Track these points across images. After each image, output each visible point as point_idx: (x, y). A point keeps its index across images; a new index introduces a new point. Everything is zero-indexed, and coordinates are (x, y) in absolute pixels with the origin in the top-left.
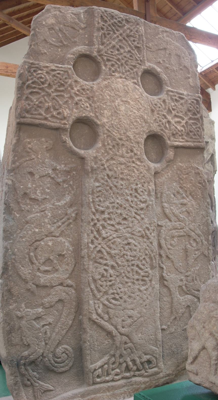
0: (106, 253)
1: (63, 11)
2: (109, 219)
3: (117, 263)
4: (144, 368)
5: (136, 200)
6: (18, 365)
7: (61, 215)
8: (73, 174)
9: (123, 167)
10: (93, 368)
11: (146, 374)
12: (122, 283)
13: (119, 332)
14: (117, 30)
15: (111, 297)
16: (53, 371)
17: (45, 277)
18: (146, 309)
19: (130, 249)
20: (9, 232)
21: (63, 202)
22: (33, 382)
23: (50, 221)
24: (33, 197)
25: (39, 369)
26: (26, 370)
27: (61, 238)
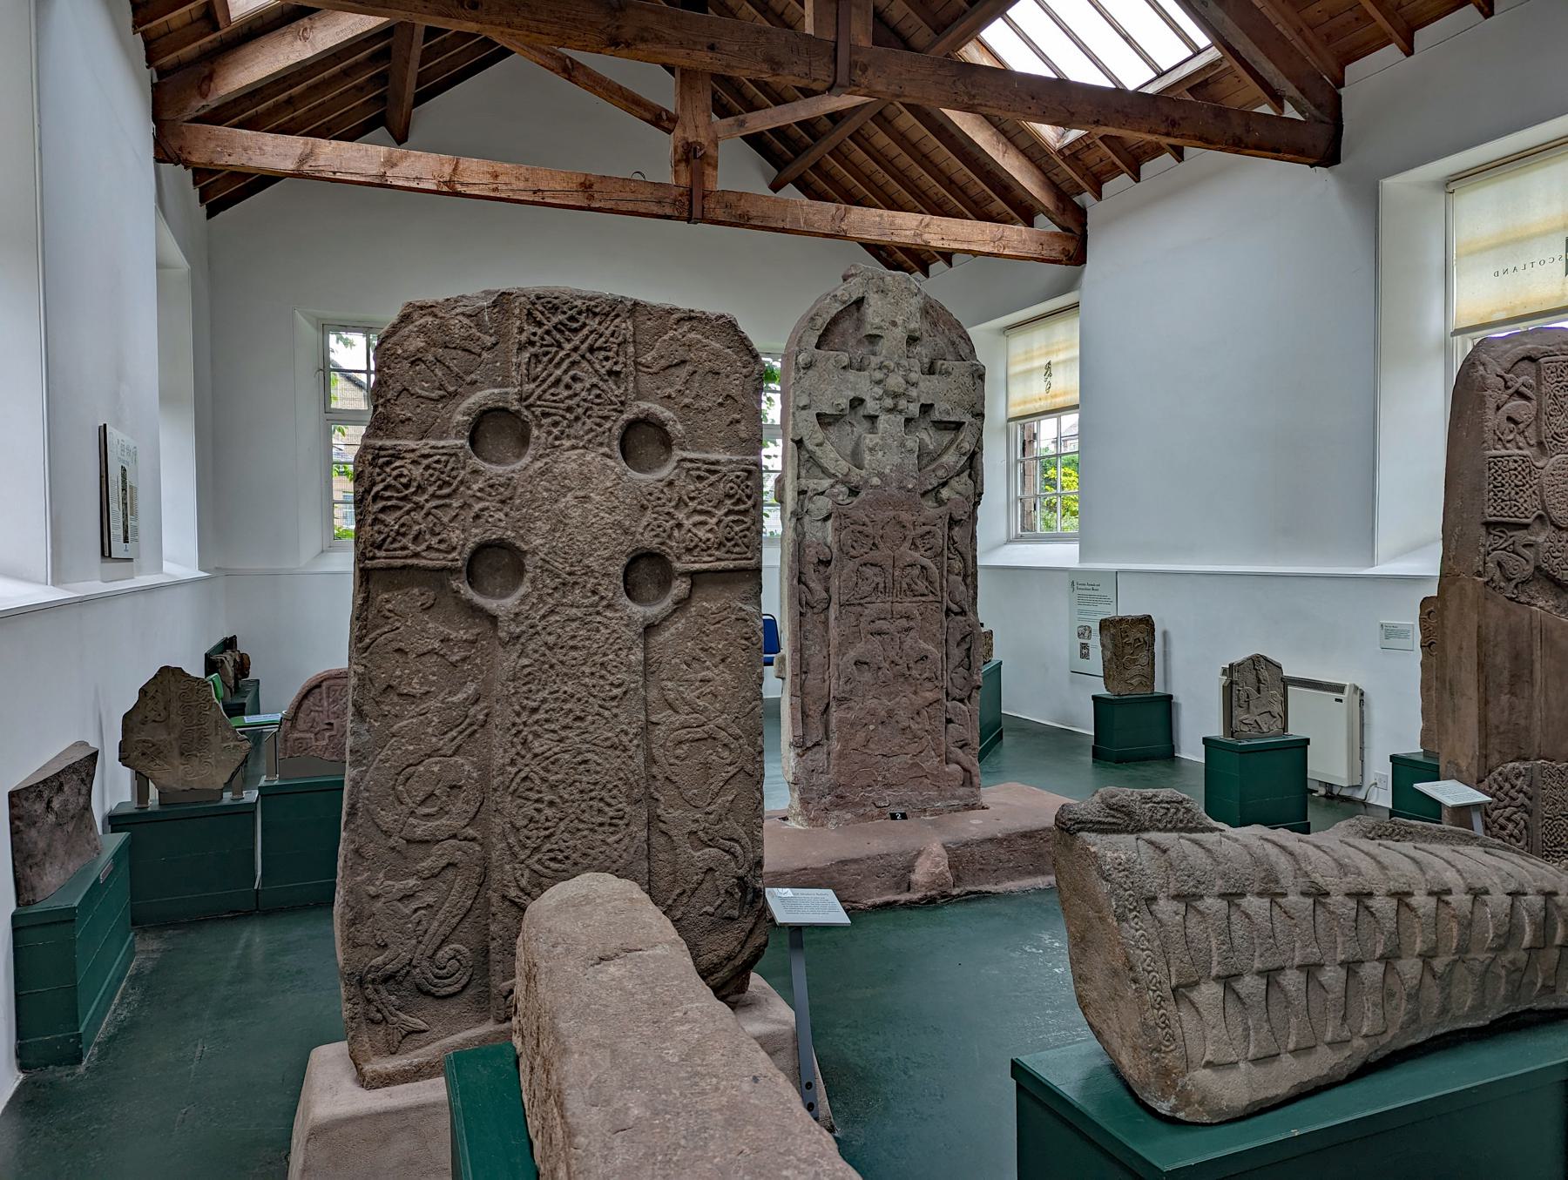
1: (440, 314)
2: (547, 721)
6: (361, 982)
8: (482, 645)
9: (574, 625)
14: (569, 341)
16: (428, 993)
19: (588, 771)
21: (461, 696)
24: (405, 691)
27: (456, 758)
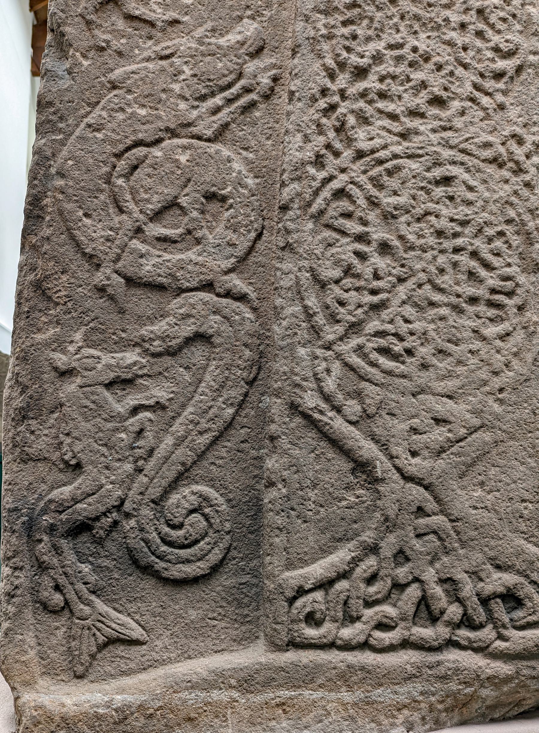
0: (364, 201)
2: (382, 95)
3: (401, 238)
4: (491, 618)
5: (479, 43)
7: (224, 76)
10: (294, 583)
11: (500, 645)
12: (416, 305)
13: (399, 470)
15: (376, 346)
17: (159, 256)
18: (501, 402)
19: (451, 198)
20: (52, 110)
22: (72, 596)
23: (186, 89)
25: (103, 554)
26: (57, 550)
